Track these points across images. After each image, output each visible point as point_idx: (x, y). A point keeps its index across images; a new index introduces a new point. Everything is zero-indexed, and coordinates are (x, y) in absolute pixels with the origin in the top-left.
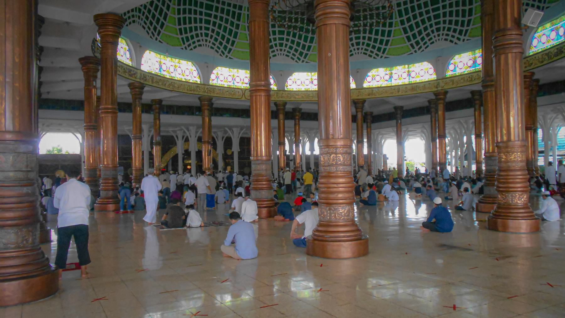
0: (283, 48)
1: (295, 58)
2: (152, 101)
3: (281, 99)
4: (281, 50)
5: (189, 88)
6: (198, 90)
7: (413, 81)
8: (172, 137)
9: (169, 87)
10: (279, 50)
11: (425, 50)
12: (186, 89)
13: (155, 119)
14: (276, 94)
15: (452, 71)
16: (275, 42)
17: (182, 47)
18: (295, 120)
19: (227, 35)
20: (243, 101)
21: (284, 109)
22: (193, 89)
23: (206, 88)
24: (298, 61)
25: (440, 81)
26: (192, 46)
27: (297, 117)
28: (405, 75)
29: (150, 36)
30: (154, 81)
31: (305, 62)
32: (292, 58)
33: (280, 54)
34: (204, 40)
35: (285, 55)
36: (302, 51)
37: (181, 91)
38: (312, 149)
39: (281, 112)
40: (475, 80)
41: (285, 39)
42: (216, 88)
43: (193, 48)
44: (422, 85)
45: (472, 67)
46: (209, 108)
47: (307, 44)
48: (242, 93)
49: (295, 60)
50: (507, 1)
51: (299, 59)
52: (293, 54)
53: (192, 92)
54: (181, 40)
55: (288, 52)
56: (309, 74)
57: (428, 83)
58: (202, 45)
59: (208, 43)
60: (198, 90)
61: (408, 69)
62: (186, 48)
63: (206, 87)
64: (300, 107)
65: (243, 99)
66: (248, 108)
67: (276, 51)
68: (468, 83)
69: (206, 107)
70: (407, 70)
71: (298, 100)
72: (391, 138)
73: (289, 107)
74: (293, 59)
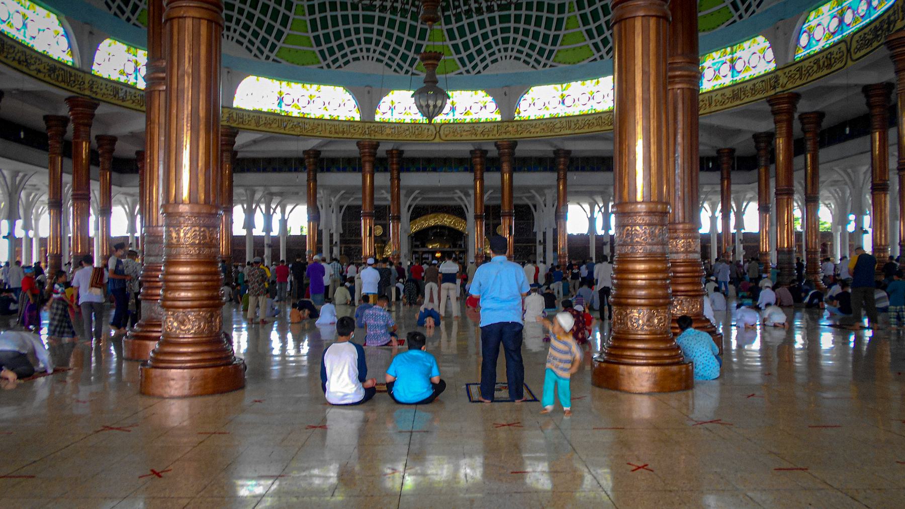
0: (510, 46)
1: (394, 65)
2: (305, 152)
3: (504, 136)
4: (506, 50)
5: (333, 129)
6: (352, 131)
7: (739, 78)
8: (528, 207)
9: (294, 130)
10: (502, 50)
11: (758, 11)
12: (328, 131)
13: (392, 179)
14: (496, 128)
15: (804, 48)
16: (495, 38)
17: (320, 65)
18: (558, 171)
19: (406, 37)
20: (436, 143)
21: (512, 154)
22: (341, 130)
23: (367, 127)
24: (536, 65)
25: (778, 73)
26: (341, 61)
27: (561, 167)
28: (725, 69)
29: (253, 54)
30: (261, 123)
31: (548, 66)
32: (525, 61)
33: (504, 58)
34: (364, 50)
35: (513, 57)
36: (544, 46)
37: (318, 134)
38: (249, 224)
39: (505, 158)
40: (835, 62)
41: (375, 31)
42: (387, 125)
43: (342, 65)
44: (750, 85)
45: (836, 34)
46: (372, 159)
47: (552, 33)
48: (434, 130)
49: (531, 65)
50: (1, 351)
51: (539, 62)
52: (390, 58)
53: (340, 135)
54: (319, 55)
55: (380, 53)
56: (559, 86)
57: (759, 80)
58: (361, 58)
59: (371, 54)
60: (352, 131)
61: (731, 56)
62: (328, 66)
63: (367, 125)
64: (402, 148)
65: (437, 140)
66: (608, 155)
67: (497, 52)
68: (826, 72)
69: (367, 158)
70: (728, 57)
71: (535, 135)
72: (303, 204)
73: (382, 151)
74: (528, 63)
